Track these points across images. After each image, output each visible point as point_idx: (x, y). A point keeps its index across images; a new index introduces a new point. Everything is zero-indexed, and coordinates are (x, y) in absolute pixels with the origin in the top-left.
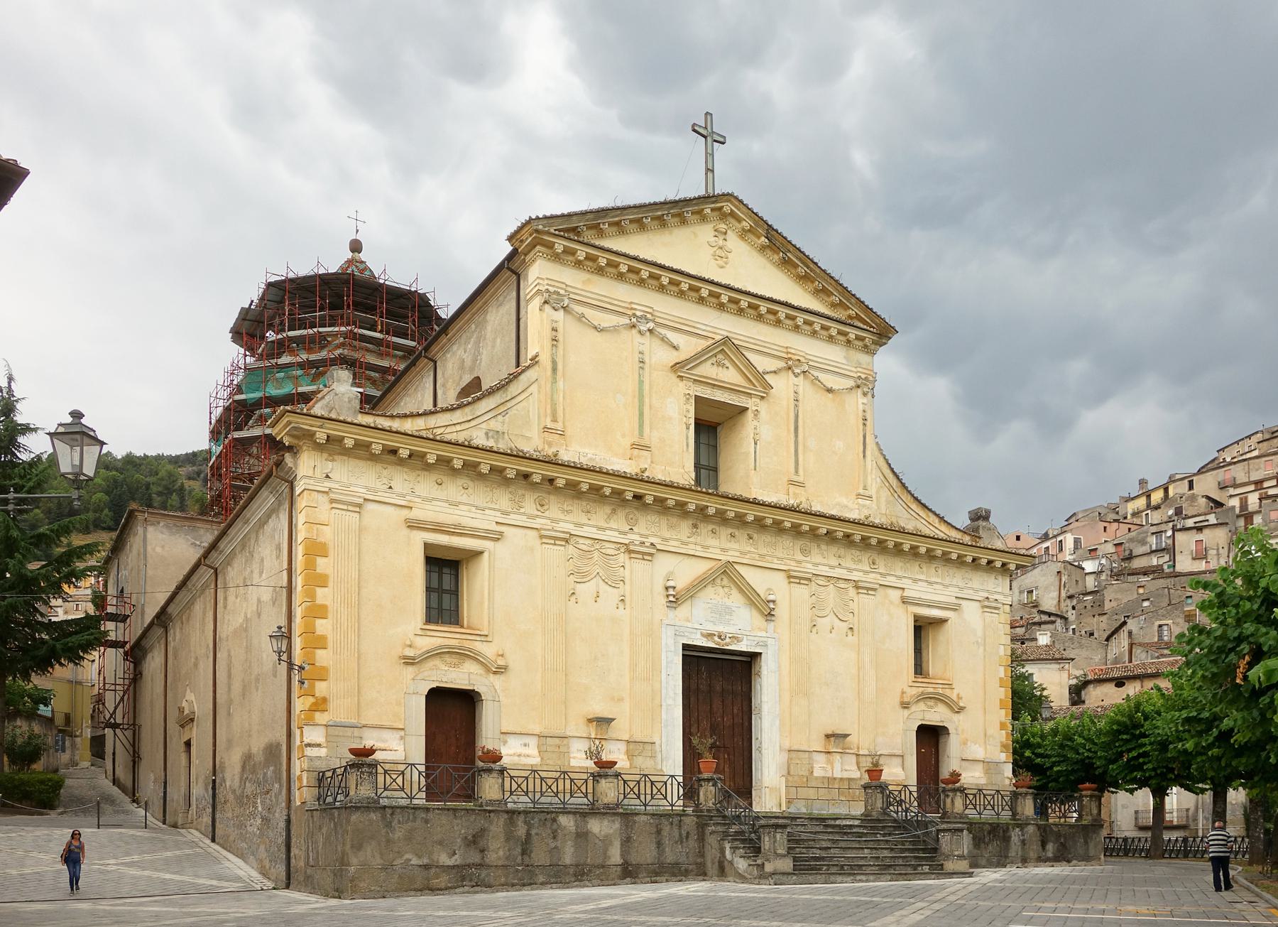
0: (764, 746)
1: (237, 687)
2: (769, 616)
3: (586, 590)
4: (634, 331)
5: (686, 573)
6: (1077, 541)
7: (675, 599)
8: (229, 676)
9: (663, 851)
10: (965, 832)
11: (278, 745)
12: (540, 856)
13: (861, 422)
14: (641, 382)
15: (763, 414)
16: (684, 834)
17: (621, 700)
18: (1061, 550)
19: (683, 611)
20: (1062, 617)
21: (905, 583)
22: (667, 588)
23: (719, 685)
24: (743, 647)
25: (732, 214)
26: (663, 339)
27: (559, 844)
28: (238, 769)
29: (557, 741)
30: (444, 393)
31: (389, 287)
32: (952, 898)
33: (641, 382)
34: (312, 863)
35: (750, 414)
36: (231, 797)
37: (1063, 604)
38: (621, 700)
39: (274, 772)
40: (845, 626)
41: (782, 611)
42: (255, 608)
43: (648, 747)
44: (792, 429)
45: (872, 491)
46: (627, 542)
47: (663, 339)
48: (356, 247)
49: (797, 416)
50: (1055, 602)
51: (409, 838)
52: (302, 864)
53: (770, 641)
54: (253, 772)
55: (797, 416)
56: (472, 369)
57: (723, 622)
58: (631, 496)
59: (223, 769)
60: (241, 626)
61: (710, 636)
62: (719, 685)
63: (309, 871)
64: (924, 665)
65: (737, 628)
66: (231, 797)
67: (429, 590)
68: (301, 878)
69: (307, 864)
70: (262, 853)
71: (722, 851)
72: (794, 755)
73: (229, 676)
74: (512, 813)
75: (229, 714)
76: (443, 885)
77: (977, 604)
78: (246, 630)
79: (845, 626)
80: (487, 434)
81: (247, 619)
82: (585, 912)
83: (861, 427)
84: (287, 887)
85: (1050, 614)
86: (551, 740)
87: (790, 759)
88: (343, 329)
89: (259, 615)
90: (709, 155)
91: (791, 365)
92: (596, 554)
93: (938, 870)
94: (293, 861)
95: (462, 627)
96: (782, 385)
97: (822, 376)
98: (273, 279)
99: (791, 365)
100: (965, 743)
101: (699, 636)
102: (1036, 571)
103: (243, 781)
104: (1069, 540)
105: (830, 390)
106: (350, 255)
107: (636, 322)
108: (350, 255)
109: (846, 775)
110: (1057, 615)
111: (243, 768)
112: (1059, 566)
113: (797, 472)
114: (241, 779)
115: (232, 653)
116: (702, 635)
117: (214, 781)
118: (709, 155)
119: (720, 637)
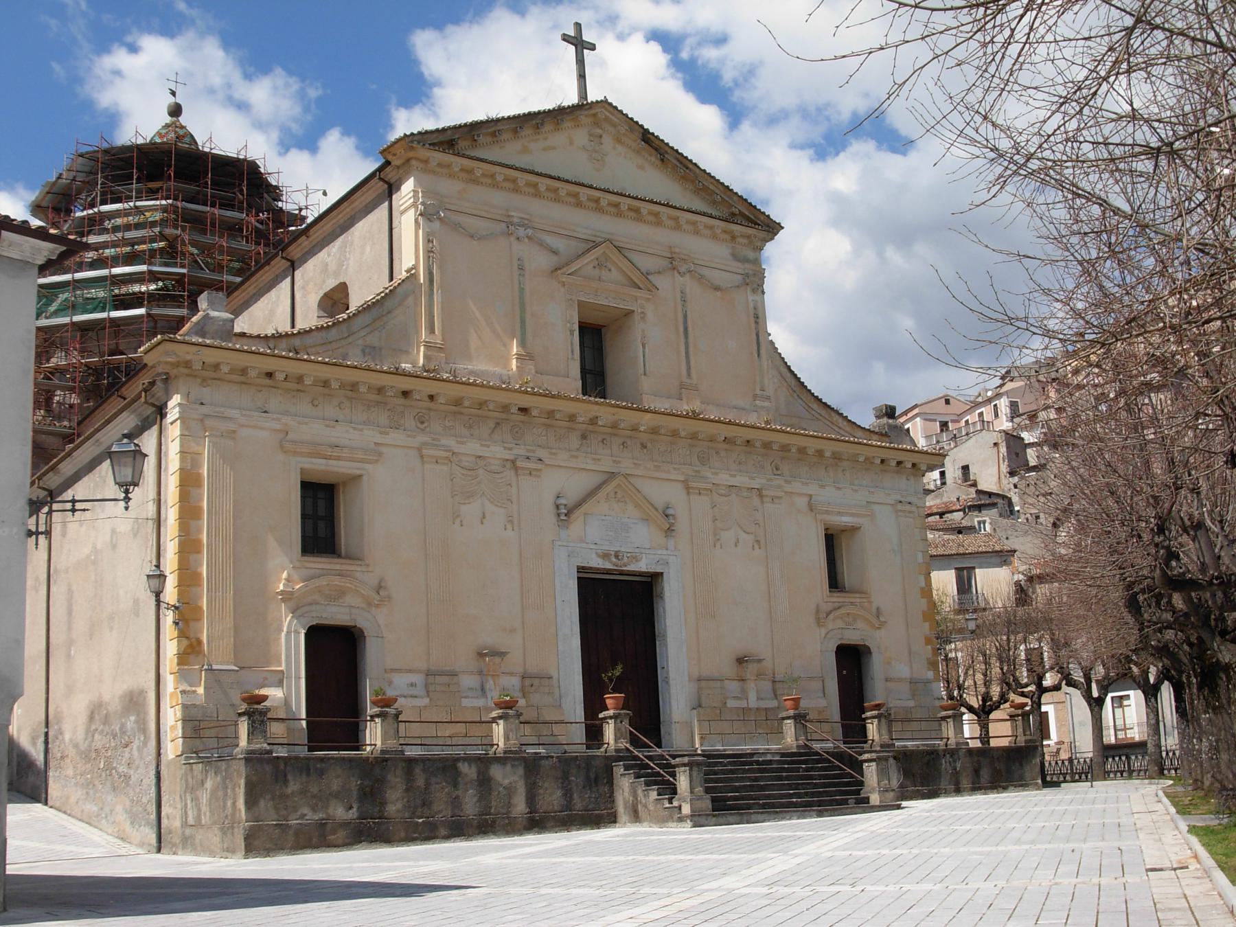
0: (672, 675)
1: (80, 625)
2: (669, 531)
3: (471, 510)
4: (512, 239)
5: (574, 485)
6: (1013, 406)
7: (565, 513)
8: (70, 612)
9: (571, 798)
10: (891, 761)
11: (142, 693)
12: (441, 808)
13: (752, 320)
14: (522, 290)
15: (650, 315)
16: (592, 776)
17: (513, 630)
18: (996, 415)
19: (577, 525)
20: (1004, 497)
21: (813, 489)
22: (558, 507)
23: (620, 616)
24: (643, 566)
25: (607, 119)
26: (541, 244)
27: (459, 793)
28: (82, 719)
29: (445, 679)
30: (304, 296)
31: (215, 157)
32: (873, 829)
33: (522, 290)
34: (191, 821)
35: (637, 317)
36: (72, 752)
37: (1004, 481)
38: (513, 630)
39: (136, 722)
40: (750, 538)
41: (682, 525)
42: (108, 537)
43: (546, 682)
44: (681, 329)
45: (770, 392)
46: (512, 458)
47: (541, 244)
48: (176, 111)
49: (685, 317)
50: (995, 479)
51: (303, 792)
52: (177, 823)
53: (671, 559)
54: (106, 720)
55: (685, 317)
56: (337, 274)
57: (619, 538)
58: (514, 413)
59: (59, 720)
60: (88, 557)
61: (605, 556)
62: (620, 616)
63: (188, 831)
64: (839, 578)
65: (640, 550)
66: (72, 752)
67: (304, 516)
68: (177, 840)
69: (185, 824)
70: (121, 817)
71: (635, 795)
72: (703, 684)
73: (70, 612)
74: (411, 761)
75: (69, 656)
76: (340, 841)
77: (889, 508)
78: (94, 563)
79: (750, 538)
80: (363, 351)
81: (95, 551)
82: (531, 845)
83: (753, 326)
84: (159, 850)
85: (990, 494)
86: (438, 679)
87: (700, 689)
88: (164, 202)
89: (114, 547)
90: (580, 62)
91: (674, 262)
92: (481, 471)
93: (863, 805)
94: (164, 822)
95: (339, 556)
96: (664, 283)
97: (706, 272)
98: (84, 149)
99: (674, 262)
100: (889, 663)
101: (594, 556)
102: (972, 441)
103: (90, 733)
104: (1003, 403)
105: (717, 289)
106: (168, 119)
107: (510, 226)
108: (168, 119)
109: (763, 704)
110: (998, 495)
111: (91, 718)
112: (995, 437)
113: (689, 375)
114: (87, 731)
115: (74, 587)
116: (598, 556)
117: (47, 734)
118: (580, 62)
119: (617, 557)
